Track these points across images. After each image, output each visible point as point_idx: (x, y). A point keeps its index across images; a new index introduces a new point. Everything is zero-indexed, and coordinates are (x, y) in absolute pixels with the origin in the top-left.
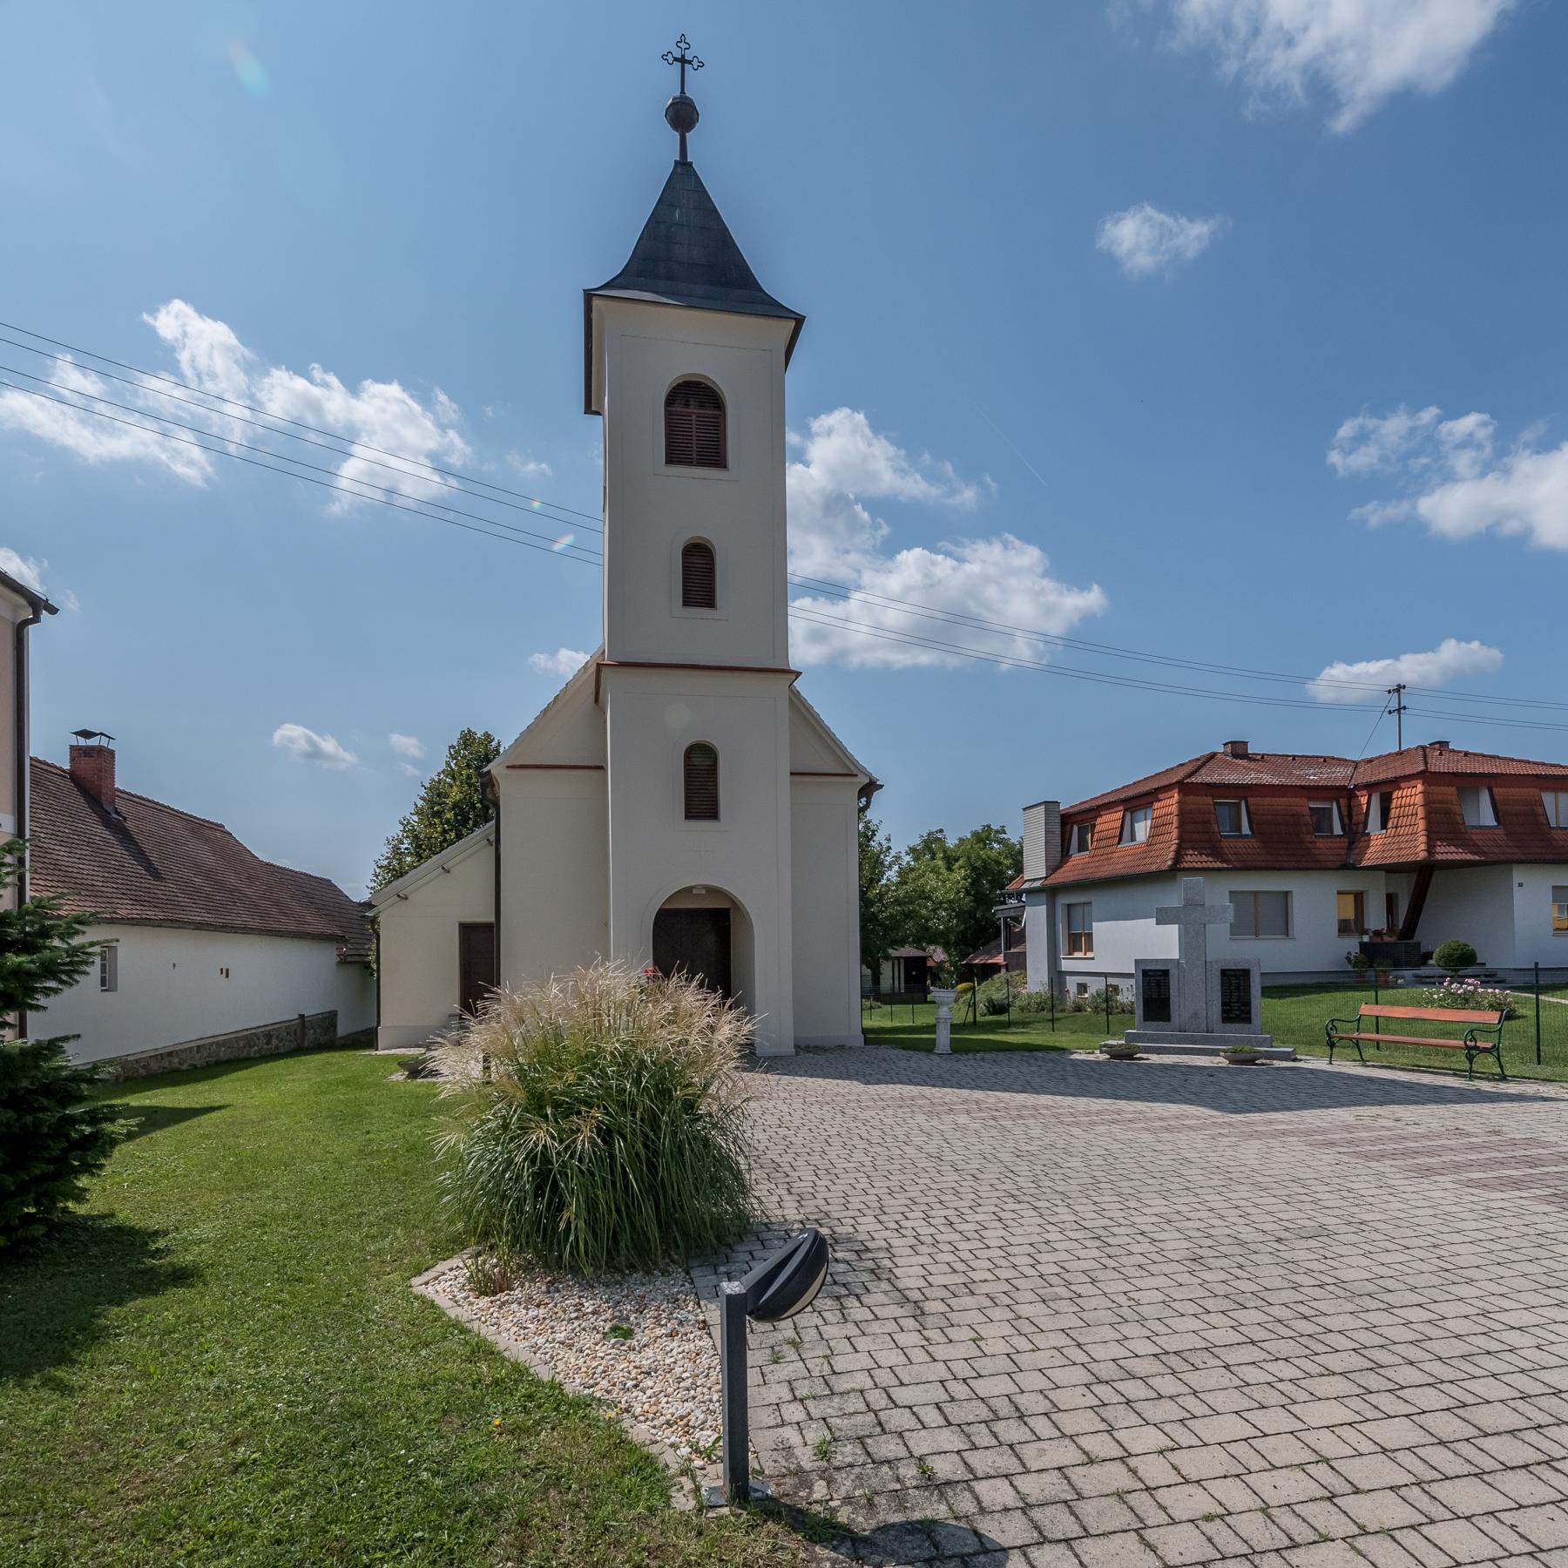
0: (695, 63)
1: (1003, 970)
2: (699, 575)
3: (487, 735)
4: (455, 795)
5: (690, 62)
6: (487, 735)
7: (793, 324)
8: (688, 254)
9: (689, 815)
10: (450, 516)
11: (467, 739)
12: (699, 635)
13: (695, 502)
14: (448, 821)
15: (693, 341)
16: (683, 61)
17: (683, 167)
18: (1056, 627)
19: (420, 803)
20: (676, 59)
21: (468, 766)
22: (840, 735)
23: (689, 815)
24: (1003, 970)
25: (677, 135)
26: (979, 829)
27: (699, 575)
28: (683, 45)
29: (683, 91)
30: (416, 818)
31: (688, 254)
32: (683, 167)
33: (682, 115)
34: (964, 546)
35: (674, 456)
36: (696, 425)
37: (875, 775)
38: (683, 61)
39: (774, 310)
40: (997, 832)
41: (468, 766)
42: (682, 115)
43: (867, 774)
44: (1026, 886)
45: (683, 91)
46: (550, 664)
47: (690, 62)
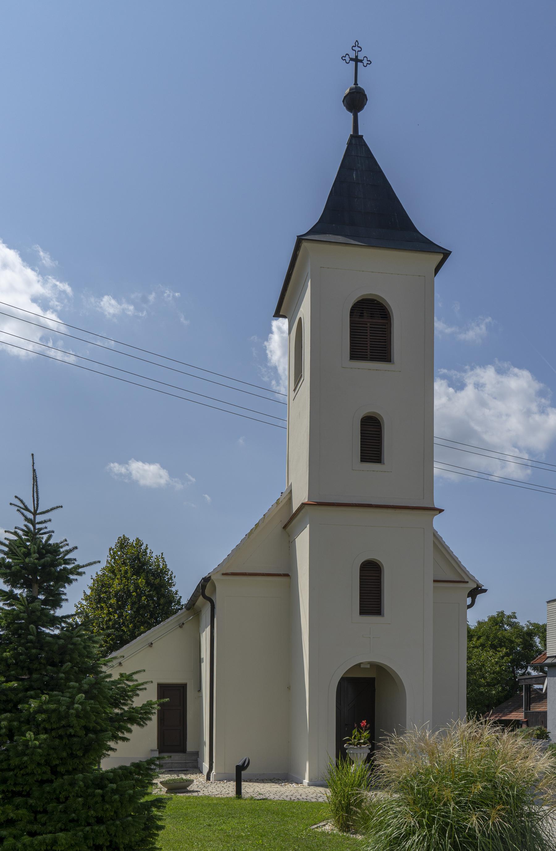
0: (365, 62)
1: (524, 727)
2: (371, 440)
3: (138, 540)
4: (116, 586)
5: (361, 61)
6: (138, 540)
7: (441, 257)
8: (363, 206)
9: (363, 612)
10: (96, 367)
11: (123, 543)
12: (372, 483)
13: (371, 386)
14: (111, 606)
15: (371, 270)
16: (356, 60)
17: (356, 142)
18: (539, 441)
19: (89, 592)
20: (351, 59)
21: (124, 563)
22: (456, 553)
23: (363, 612)
24: (524, 727)
25: (351, 115)
26: (495, 614)
27: (371, 440)
28: (357, 49)
29: (356, 83)
30: (84, 603)
31: (363, 206)
32: (356, 142)
33: (355, 100)
34: (465, 371)
35: (357, 353)
36: (370, 330)
37: (481, 582)
38: (356, 60)
39: (425, 245)
40: (509, 617)
41: (124, 563)
42: (355, 100)
43: (475, 581)
44: (549, 661)
45: (356, 83)
46: (123, 470)
47: (361, 61)
